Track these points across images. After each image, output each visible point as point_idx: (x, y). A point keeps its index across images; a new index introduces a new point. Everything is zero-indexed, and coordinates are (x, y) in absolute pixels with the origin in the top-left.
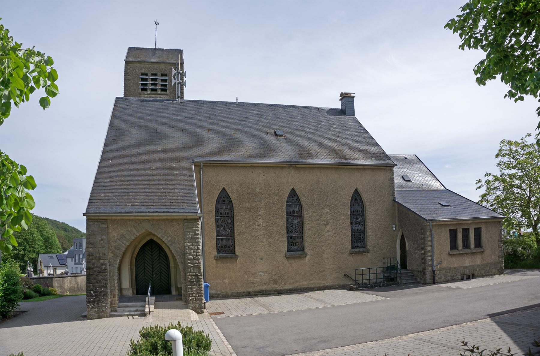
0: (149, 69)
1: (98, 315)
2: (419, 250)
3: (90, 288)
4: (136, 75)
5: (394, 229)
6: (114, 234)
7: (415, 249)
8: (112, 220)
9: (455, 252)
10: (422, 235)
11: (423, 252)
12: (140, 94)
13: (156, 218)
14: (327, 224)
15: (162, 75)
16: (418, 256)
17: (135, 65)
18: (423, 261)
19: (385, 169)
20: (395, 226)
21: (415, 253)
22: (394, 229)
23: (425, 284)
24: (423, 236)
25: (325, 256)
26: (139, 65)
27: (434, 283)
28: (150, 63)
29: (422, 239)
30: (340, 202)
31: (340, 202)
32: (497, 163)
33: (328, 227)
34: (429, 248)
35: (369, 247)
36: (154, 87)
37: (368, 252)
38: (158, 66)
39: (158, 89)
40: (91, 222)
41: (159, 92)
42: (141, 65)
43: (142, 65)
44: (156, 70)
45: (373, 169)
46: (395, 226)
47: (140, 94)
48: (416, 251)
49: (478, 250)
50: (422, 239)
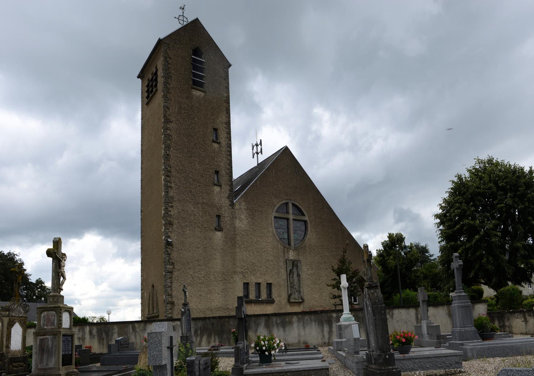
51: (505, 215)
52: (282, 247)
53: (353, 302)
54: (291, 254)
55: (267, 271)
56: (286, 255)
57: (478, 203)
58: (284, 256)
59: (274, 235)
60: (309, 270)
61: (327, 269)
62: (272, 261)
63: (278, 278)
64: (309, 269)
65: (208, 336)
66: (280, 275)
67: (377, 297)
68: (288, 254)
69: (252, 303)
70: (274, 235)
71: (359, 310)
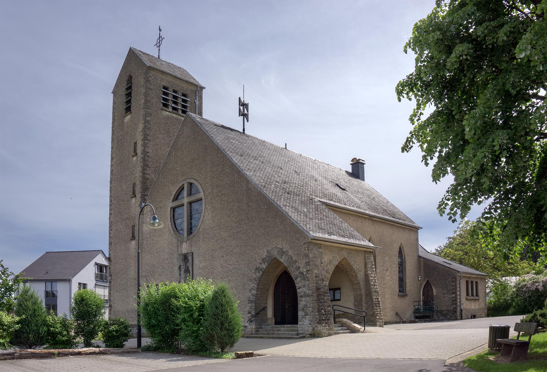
0: (171, 84)
1: (329, 333)
2: (449, 294)
3: (321, 308)
4: (158, 86)
5: (420, 279)
6: (326, 259)
7: (445, 294)
8: (324, 245)
9: (468, 298)
10: (453, 282)
11: (454, 295)
12: (162, 109)
13: (354, 248)
14: (387, 270)
15: (184, 95)
16: (448, 299)
17: (157, 74)
18: (454, 302)
19: (414, 230)
20: (420, 276)
21: (445, 297)
22: (420, 279)
23: (456, 319)
24: (454, 284)
25: (387, 296)
26: (161, 75)
27: (462, 319)
28: (173, 77)
29: (453, 286)
30: (394, 253)
31: (394, 253)
32: (450, 238)
33: (388, 272)
34: (458, 293)
35: (407, 293)
36: (175, 105)
37: (406, 295)
38: (179, 83)
39: (179, 109)
40: (312, 245)
41: (180, 112)
42: (164, 76)
43: (164, 77)
44: (178, 87)
45: (409, 229)
46: (420, 276)
47: (162, 109)
48: (446, 295)
49: (477, 298)
50: (453, 286)
51: (541, 105)
52: (176, 241)
53: (496, 205)
54: (185, 247)
55: (163, 271)
56: (180, 249)
57: (236, 250)
58: (178, 251)
59: (170, 230)
60: (201, 263)
61: (223, 257)
62: (167, 259)
63: (172, 277)
64: (201, 261)
65: (454, 191)
66: (174, 273)
67: (109, 340)
68: (182, 247)
69: (68, 355)
70: (170, 230)
71: (61, 355)
